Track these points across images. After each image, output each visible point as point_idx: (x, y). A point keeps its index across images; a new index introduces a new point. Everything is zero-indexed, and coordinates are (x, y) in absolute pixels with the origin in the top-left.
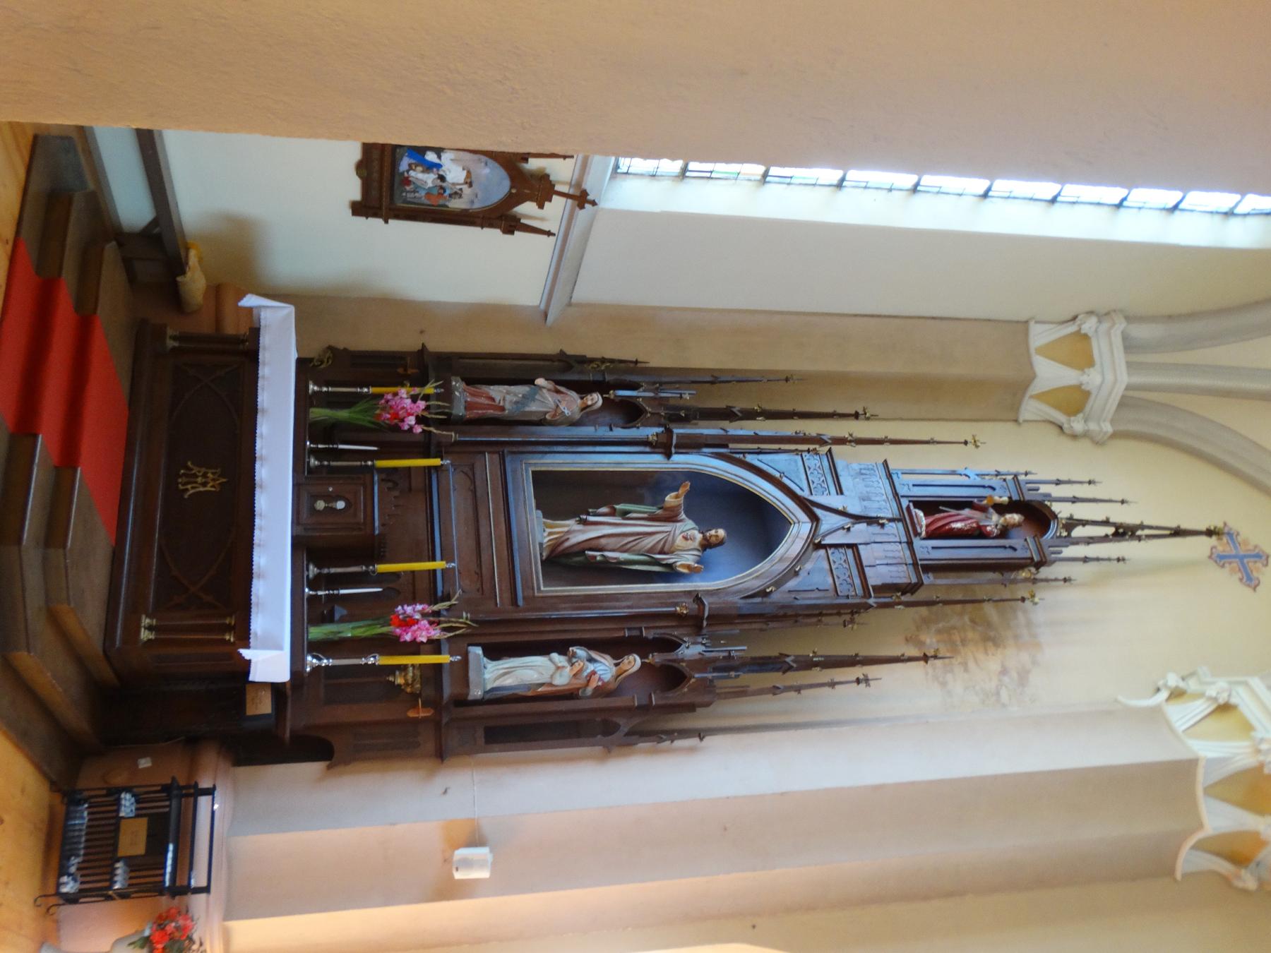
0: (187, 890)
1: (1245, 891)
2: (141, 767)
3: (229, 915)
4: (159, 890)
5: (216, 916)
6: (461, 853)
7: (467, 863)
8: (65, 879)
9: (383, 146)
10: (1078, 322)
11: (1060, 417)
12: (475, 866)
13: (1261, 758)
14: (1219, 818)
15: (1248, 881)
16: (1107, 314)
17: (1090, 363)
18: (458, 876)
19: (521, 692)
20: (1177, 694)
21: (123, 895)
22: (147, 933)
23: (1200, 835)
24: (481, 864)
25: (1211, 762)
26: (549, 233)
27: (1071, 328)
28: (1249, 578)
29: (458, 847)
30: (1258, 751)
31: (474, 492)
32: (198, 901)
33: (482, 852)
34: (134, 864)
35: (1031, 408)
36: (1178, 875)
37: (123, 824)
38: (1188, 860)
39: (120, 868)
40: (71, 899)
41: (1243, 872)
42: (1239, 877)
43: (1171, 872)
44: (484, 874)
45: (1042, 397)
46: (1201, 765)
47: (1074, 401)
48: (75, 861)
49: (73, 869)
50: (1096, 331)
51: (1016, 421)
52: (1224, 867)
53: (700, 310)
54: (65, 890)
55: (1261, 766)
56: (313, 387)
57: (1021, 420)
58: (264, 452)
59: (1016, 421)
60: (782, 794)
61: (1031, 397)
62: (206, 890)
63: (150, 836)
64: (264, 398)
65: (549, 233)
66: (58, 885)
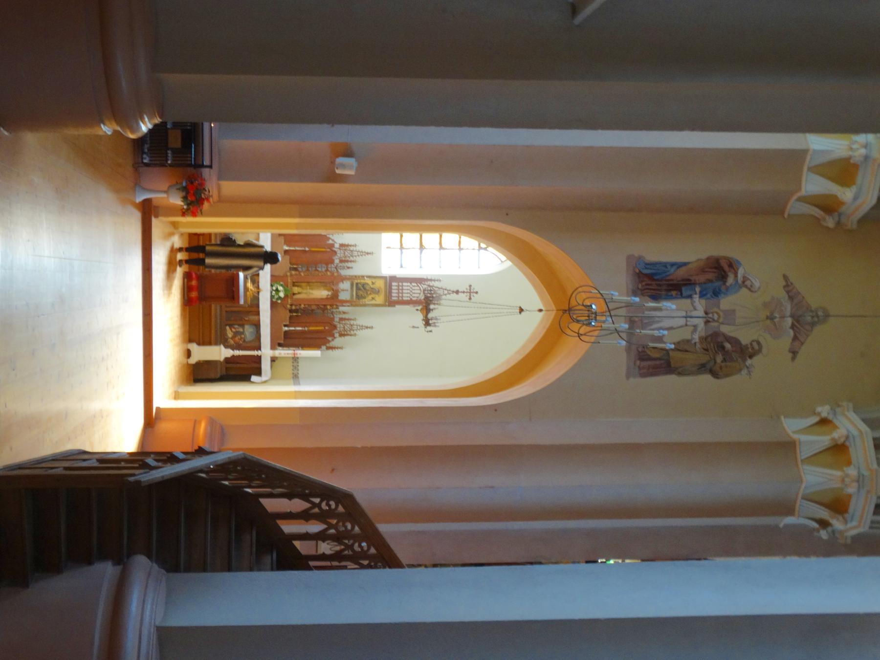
0: (203, 166)
1: (827, 228)
3: (220, 177)
4: (190, 165)
5: (214, 178)
6: (340, 160)
7: (343, 166)
8: (145, 156)
12: (347, 167)
13: (850, 153)
14: (814, 185)
15: (830, 222)
18: (338, 171)
19: (58, 457)
21: (170, 165)
22: (184, 184)
23: (798, 194)
24: (351, 167)
25: (815, 151)
29: (338, 157)
30: (851, 149)
31: (144, 601)
32: (206, 172)
33: (351, 161)
34: (175, 151)
36: (786, 216)
37: (169, 131)
38: (794, 207)
39: (169, 152)
40: (147, 165)
41: (827, 217)
42: (824, 220)
43: (782, 212)
44: (351, 172)
46: (810, 153)
48: (146, 146)
49: (146, 150)
52: (817, 212)
53: (115, 453)
54: (145, 161)
55: (850, 158)
60: (527, 146)
62: (210, 167)
63: (183, 139)
66: (142, 159)
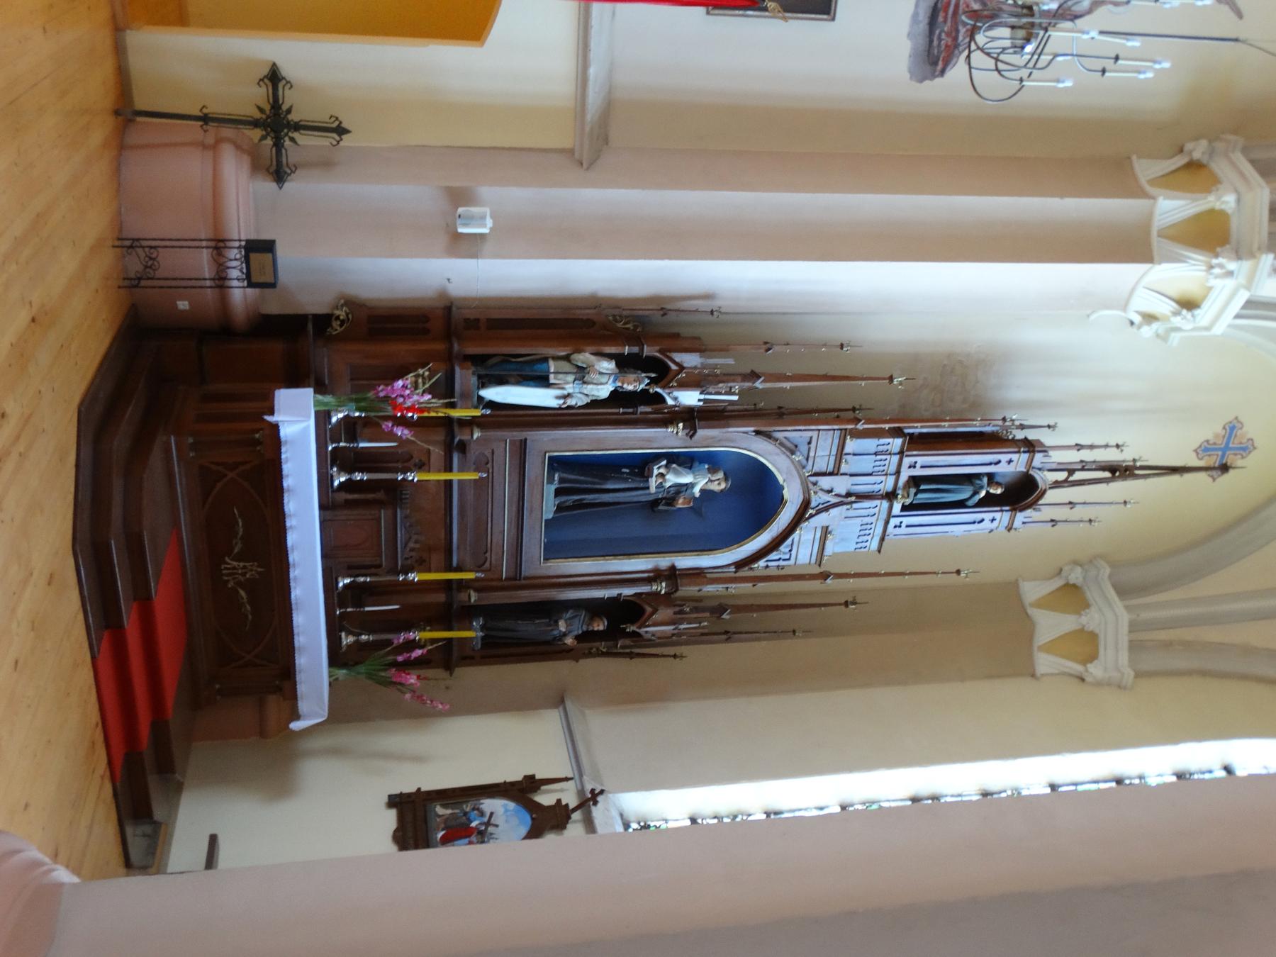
2: (186, 303)
9: (417, 847)
10: (1064, 574)
11: (1077, 668)
16: (1091, 562)
17: (1088, 606)
20: (1149, 318)
26: (567, 779)
27: (1058, 583)
28: (1244, 449)
35: (1045, 663)
45: (1050, 648)
47: (1071, 596)
50: (1084, 578)
51: (1033, 676)
56: (347, 640)
57: (1038, 673)
58: (297, 559)
59: (1033, 676)
61: (1040, 648)
64: (296, 593)
65: (567, 779)
